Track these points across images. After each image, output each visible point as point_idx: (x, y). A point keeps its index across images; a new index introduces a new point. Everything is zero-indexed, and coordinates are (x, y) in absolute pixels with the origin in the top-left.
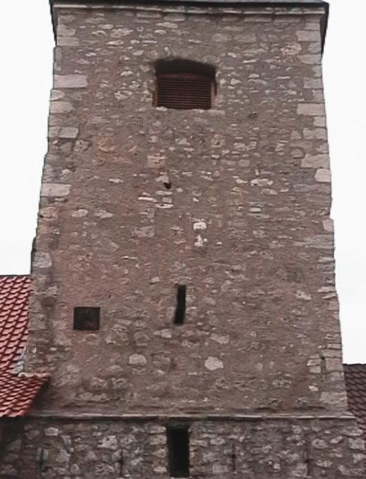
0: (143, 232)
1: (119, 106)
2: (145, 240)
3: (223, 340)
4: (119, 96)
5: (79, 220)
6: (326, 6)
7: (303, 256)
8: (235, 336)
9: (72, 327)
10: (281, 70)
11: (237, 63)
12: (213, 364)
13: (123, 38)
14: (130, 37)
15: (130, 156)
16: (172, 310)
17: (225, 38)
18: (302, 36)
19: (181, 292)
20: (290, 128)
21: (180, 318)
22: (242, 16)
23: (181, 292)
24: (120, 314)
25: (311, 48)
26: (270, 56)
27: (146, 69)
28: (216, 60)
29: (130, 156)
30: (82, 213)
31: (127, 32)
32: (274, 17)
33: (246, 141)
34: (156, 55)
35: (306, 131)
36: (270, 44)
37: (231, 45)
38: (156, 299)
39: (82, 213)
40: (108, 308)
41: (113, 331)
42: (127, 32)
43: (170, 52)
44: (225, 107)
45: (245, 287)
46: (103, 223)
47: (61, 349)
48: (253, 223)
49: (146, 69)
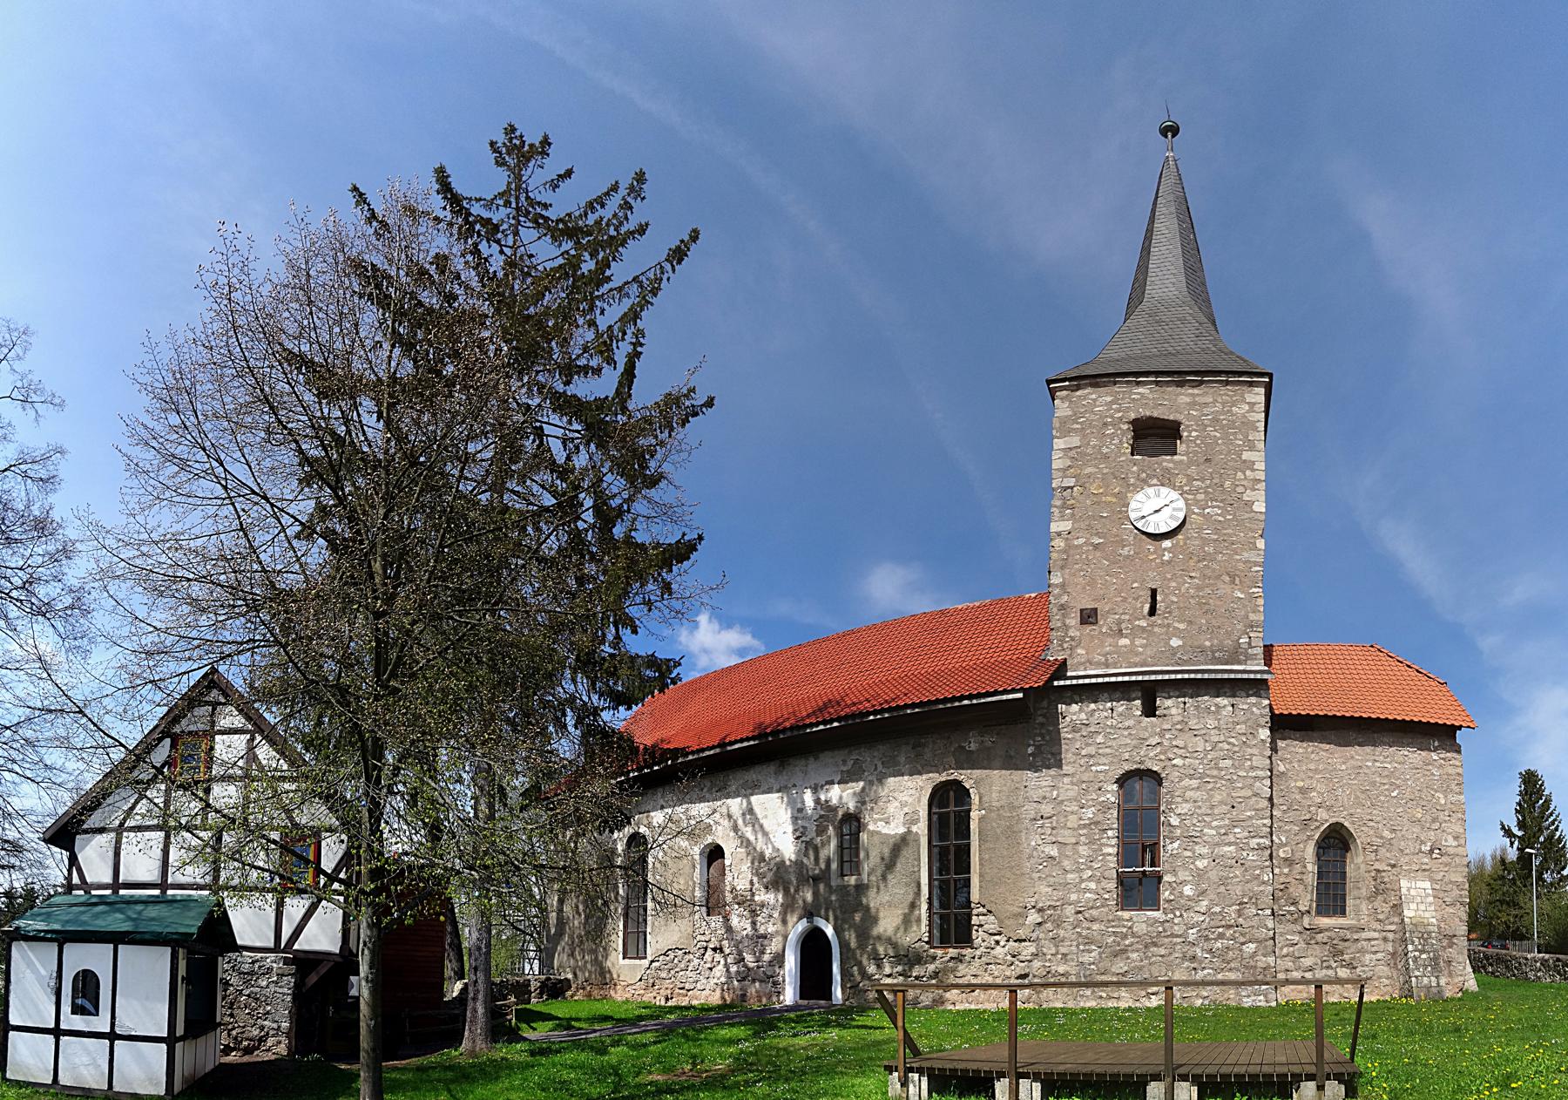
0: (1125, 551)
1: (1106, 457)
2: (1128, 557)
3: (1182, 626)
4: (1105, 450)
5: (1080, 546)
6: (1270, 376)
7: (1241, 566)
8: (1190, 623)
9: (1112, 898)
10: (1232, 425)
11: (1197, 419)
12: (1175, 642)
13: (1106, 404)
14: (1112, 403)
15: (1115, 495)
16: (1147, 607)
17: (1188, 400)
18: (1250, 398)
19: (1154, 593)
20: (1236, 470)
21: (1152, 612)
22: (1202, 382)
23: (1154, 593)
24: (1112, 612)
25: (1256, 408)
26: (1223, 413)
27: (1125, 427)
28: (1179, 417)
29: (1115, 495)
30: (1081, 541)
31: (1109, 399)
32: (1227, 383)
33: (1203, 480)
34: (1133, 416)
35: (1248, 473)
36: (1223, 404)
37: (1193, 405)
38: (1136, 599)
39: (1081, 541)
40: (1103, 608)
41: (1104, 625)
42: (1109, 399)
43: (1146, 412)
44: (1187, 454)
45: (1199, 588)
46: (1096, 547)
47: (1072, 639)
48: (1205, 542)
49: (1125, 427)
